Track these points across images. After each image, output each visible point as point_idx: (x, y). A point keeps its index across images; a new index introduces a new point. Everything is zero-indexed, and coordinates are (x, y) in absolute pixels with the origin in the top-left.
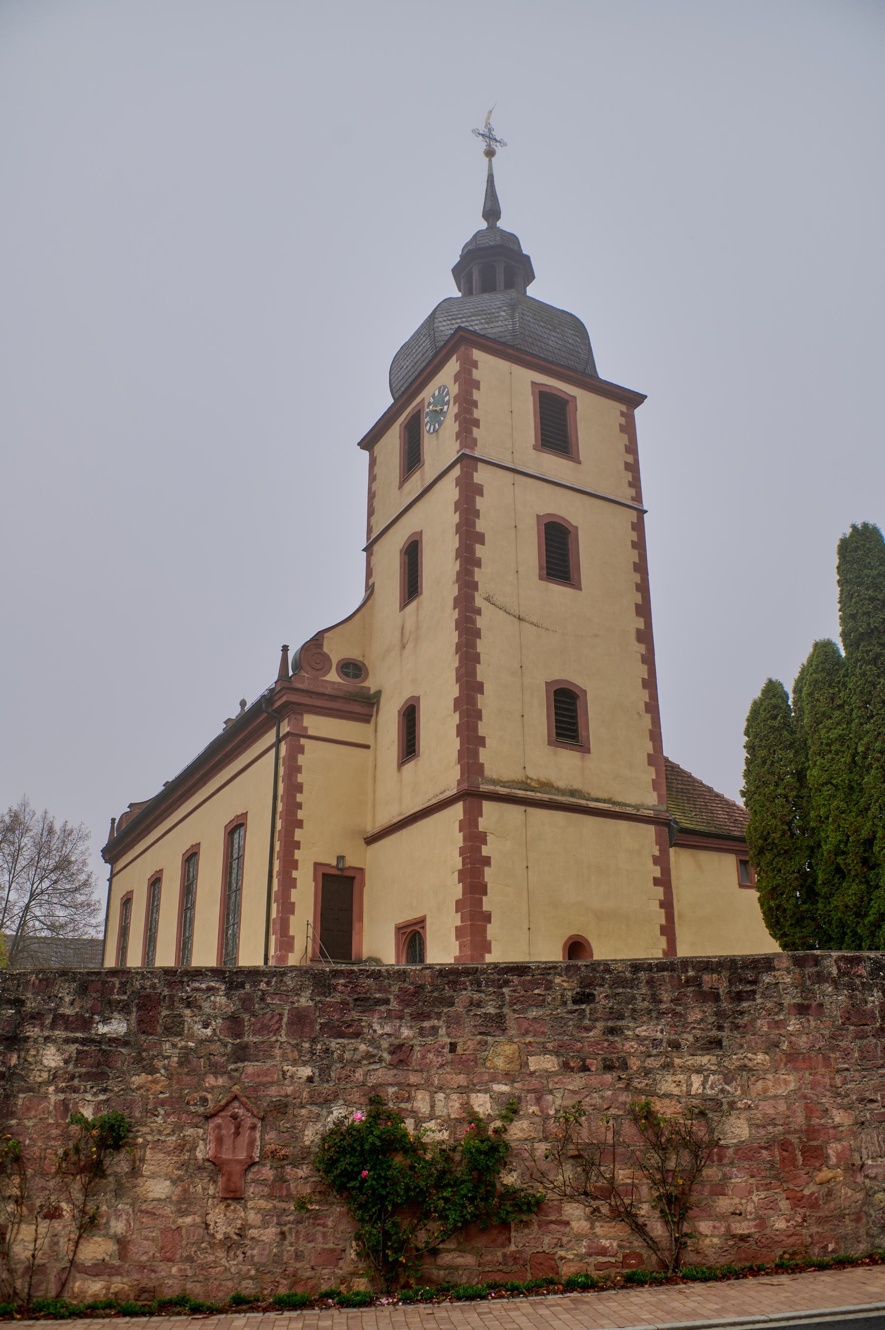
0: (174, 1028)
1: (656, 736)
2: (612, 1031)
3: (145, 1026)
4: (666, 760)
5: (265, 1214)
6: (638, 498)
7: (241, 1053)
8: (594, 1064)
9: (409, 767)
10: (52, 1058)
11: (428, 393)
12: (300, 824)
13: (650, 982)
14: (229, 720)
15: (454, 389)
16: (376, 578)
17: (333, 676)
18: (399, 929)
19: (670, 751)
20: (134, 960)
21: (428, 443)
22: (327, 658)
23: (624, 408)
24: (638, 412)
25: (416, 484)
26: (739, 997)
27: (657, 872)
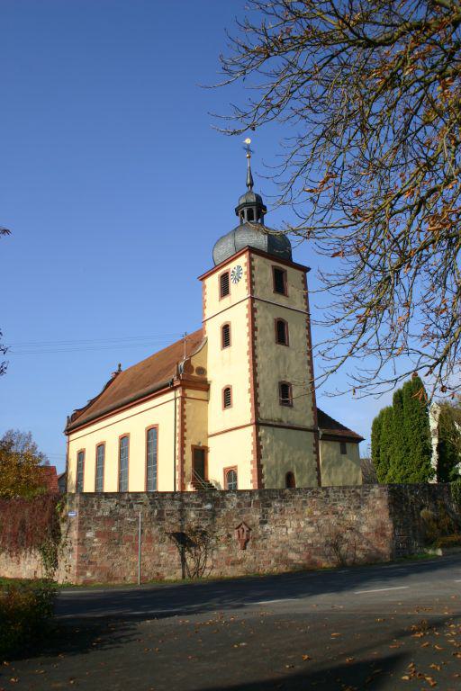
0: (224, 506)
1: (314, 401)
2: (334, 504)
3: (216, 505)
4: (318, 409)
5: (251, 553)
6: (308, 309)
7: (241, 512)
8: (330, 513)
9: (227, 411)
10: (192, 515)
11: (232, 266)
12: (186, 431)
13: (343, 492)
14: (248, 352)
15: (245, 269)
16: (260, 378)
17: (194, 374)
18: (225, 470)
19: (318, 406)
20: (137, 484)
21: (232, 286)
22: (192, 367)
23: (302, 273)
24: (307, 273)
25: (227, 301)
26: (365, 495)
27: (315, 449)
